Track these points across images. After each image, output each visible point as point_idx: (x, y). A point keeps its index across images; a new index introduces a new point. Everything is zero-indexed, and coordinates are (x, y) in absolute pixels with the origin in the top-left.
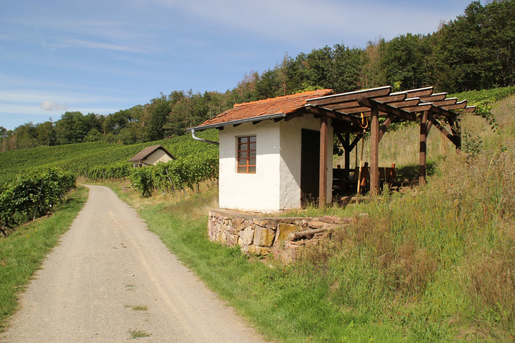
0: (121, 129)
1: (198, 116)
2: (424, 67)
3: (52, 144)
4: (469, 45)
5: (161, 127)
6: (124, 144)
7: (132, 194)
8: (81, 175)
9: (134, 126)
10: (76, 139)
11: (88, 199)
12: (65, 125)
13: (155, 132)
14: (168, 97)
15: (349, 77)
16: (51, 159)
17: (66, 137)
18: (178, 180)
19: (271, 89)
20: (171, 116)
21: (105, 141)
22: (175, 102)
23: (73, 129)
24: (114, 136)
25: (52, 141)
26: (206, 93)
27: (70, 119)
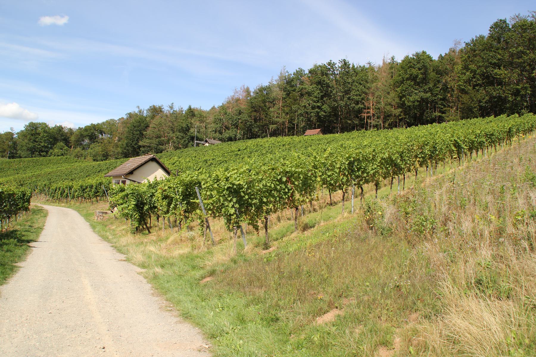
0: (91, 144)
1: (180, 132)
2: (439, 89)
3: (12, 156)
4: (498, 66)
5: (136, 144)
6: (94, 160)
7: (112, 223)
8: (41, 193)
9: (106, 141)
10: (39, 152)
11: (44, 233)
12: (28, 137)
13: (130, 148)
14: (145, 112)
15: (356, 95)
16: (9, 173)
17: (28, 150)
18: (232, 211)
19: (265, 106)
20: (149, 132)
21: (72, 156)
22: (153, 117)
23: (37, 142)
24: (83, 152)
25: (12, 153)
26: (190, 108)
27: (34, 131)
